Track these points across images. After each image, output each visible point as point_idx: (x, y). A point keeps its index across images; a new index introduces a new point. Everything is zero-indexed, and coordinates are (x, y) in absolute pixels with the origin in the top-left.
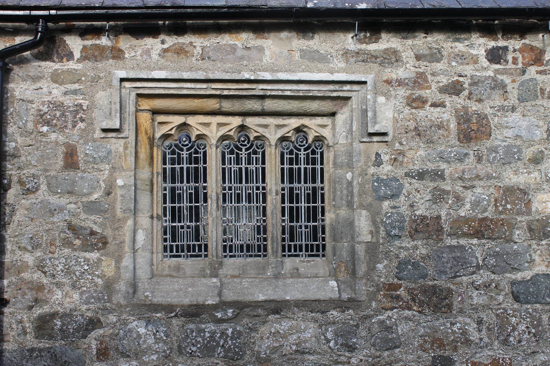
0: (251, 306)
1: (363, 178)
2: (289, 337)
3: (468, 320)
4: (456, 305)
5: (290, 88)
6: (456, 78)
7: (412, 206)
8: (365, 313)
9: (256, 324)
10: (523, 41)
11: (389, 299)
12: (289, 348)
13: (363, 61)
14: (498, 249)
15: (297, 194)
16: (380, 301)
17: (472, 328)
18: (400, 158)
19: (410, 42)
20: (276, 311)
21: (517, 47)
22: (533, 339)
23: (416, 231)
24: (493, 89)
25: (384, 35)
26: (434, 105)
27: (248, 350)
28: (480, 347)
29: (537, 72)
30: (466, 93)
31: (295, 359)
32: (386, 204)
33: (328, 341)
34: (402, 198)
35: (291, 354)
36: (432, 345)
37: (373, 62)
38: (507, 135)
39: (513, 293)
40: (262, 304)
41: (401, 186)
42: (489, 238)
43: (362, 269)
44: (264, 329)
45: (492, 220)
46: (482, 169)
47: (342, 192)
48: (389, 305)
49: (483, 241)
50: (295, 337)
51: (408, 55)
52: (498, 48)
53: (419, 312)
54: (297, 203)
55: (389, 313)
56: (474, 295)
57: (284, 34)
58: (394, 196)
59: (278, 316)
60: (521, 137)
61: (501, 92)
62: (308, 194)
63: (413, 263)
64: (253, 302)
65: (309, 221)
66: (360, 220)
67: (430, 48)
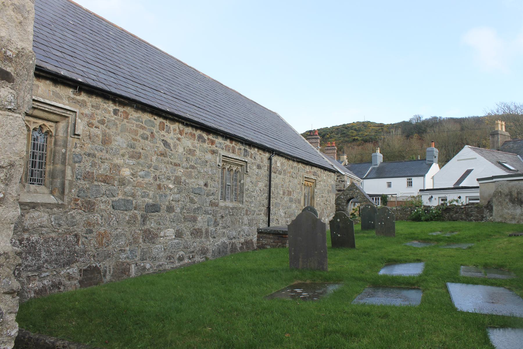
0: (24, 204)
1: (70, 152)
2: (37, 220)
3: (99, 215)
4: (96, 209)
5: (48, 107)
6: (103, 118)
7: (85, 167)
8: (66, 210)
9: (24, 213)
10: (124, 109)
11: (75, 205)
12: (37, 225)
13: (75, 103)
14: (109, 188)
15: (36, 155)
16: (72, 205)
17: (99, 218)
18: (83, 146)
19: (90, 99)
20: (34, 208)
21: (122, 111)
22: (117, 223)
23: (86, 177)
24: (114, 125)
25: (82, 93)
26: (96, 127)
27: (20, 225)
28: (101, 226)
29: (127, 122)
30: (106, 124)
31: (39, 230)
32: (77, 165)
33: (52, 222)
34: (82, 163)
35: (37, 227)
36: (87, 225)
37: (78, 104)
38: (116, 144)
39: (112, 205)
40: (29, 204)
41: (82, 159)
42: (107, 183)
43: (67, 191)
44: (27, 216)
45: (109, 176)
46: (108, 156)
47: (59, 157)
48: (74, 207)
49: (106, 184)
50: (40, 219)
51: (89, 104)
52: (117, 110)
53: (84, 211)
54: (35, 159)
55: (74, 211)
56: (101, 205)
57: (48, 82)
58: (80, 162)
59: (34, 210)
60: (120, 145)
61: (115, 127)
62: (40, 156)
63: (84, 190)
64: (25, 203)
65: (39, 168)
66: (68, 170)
67: (97, 104)
